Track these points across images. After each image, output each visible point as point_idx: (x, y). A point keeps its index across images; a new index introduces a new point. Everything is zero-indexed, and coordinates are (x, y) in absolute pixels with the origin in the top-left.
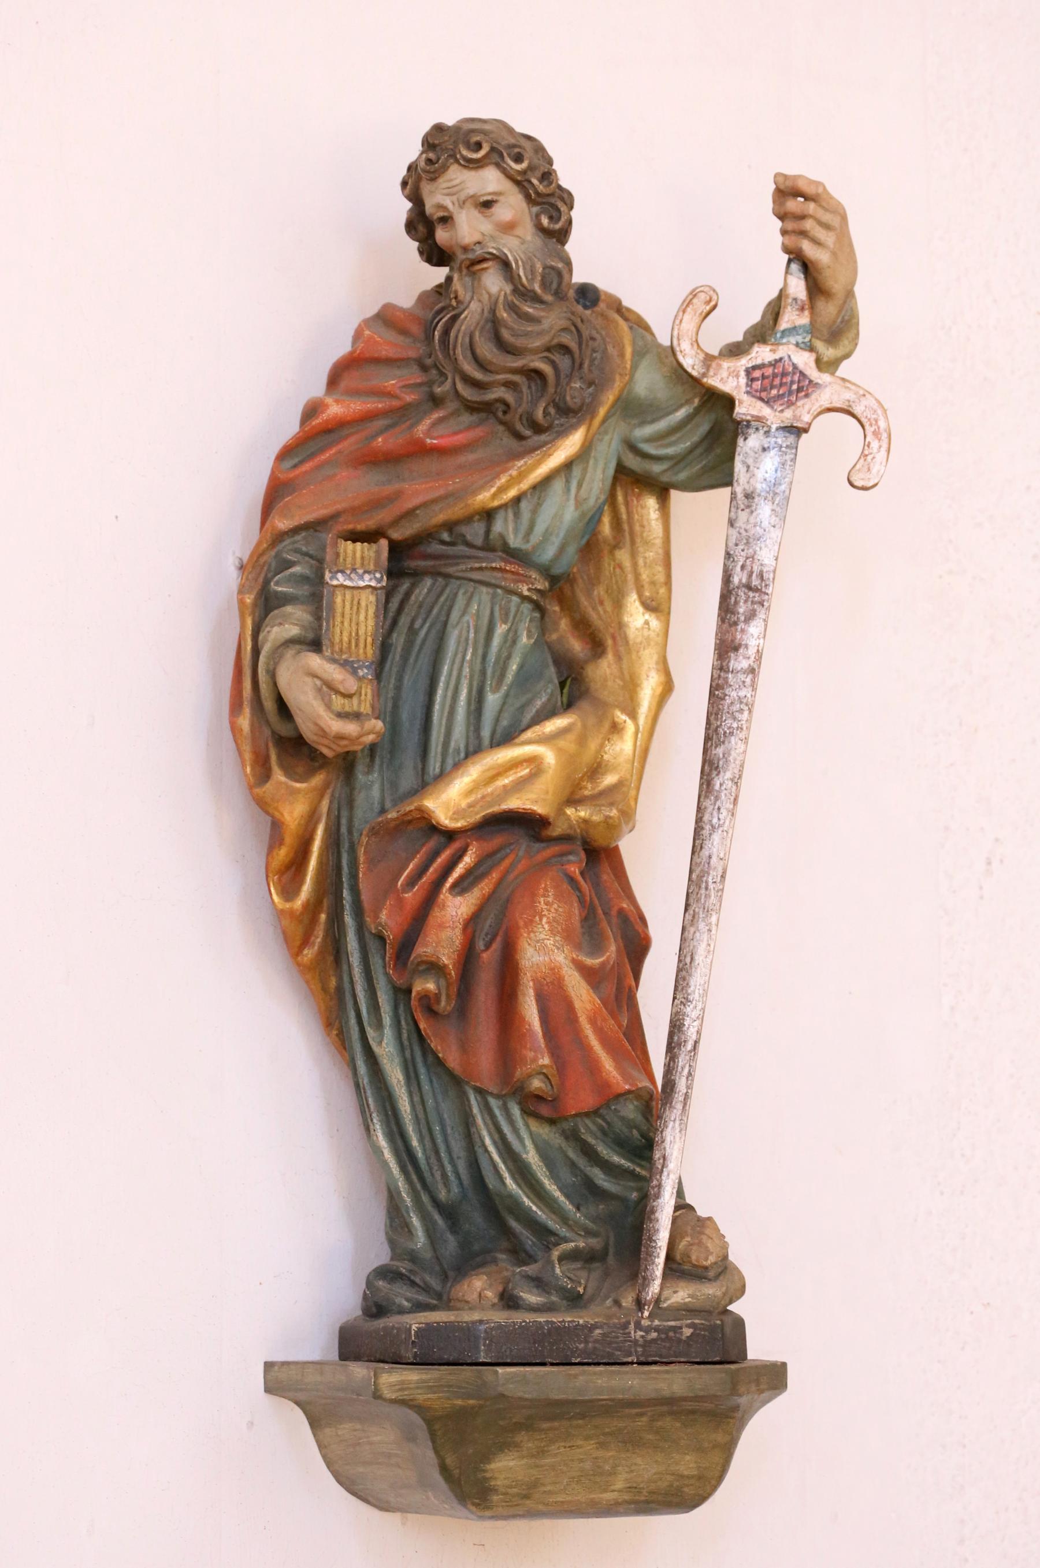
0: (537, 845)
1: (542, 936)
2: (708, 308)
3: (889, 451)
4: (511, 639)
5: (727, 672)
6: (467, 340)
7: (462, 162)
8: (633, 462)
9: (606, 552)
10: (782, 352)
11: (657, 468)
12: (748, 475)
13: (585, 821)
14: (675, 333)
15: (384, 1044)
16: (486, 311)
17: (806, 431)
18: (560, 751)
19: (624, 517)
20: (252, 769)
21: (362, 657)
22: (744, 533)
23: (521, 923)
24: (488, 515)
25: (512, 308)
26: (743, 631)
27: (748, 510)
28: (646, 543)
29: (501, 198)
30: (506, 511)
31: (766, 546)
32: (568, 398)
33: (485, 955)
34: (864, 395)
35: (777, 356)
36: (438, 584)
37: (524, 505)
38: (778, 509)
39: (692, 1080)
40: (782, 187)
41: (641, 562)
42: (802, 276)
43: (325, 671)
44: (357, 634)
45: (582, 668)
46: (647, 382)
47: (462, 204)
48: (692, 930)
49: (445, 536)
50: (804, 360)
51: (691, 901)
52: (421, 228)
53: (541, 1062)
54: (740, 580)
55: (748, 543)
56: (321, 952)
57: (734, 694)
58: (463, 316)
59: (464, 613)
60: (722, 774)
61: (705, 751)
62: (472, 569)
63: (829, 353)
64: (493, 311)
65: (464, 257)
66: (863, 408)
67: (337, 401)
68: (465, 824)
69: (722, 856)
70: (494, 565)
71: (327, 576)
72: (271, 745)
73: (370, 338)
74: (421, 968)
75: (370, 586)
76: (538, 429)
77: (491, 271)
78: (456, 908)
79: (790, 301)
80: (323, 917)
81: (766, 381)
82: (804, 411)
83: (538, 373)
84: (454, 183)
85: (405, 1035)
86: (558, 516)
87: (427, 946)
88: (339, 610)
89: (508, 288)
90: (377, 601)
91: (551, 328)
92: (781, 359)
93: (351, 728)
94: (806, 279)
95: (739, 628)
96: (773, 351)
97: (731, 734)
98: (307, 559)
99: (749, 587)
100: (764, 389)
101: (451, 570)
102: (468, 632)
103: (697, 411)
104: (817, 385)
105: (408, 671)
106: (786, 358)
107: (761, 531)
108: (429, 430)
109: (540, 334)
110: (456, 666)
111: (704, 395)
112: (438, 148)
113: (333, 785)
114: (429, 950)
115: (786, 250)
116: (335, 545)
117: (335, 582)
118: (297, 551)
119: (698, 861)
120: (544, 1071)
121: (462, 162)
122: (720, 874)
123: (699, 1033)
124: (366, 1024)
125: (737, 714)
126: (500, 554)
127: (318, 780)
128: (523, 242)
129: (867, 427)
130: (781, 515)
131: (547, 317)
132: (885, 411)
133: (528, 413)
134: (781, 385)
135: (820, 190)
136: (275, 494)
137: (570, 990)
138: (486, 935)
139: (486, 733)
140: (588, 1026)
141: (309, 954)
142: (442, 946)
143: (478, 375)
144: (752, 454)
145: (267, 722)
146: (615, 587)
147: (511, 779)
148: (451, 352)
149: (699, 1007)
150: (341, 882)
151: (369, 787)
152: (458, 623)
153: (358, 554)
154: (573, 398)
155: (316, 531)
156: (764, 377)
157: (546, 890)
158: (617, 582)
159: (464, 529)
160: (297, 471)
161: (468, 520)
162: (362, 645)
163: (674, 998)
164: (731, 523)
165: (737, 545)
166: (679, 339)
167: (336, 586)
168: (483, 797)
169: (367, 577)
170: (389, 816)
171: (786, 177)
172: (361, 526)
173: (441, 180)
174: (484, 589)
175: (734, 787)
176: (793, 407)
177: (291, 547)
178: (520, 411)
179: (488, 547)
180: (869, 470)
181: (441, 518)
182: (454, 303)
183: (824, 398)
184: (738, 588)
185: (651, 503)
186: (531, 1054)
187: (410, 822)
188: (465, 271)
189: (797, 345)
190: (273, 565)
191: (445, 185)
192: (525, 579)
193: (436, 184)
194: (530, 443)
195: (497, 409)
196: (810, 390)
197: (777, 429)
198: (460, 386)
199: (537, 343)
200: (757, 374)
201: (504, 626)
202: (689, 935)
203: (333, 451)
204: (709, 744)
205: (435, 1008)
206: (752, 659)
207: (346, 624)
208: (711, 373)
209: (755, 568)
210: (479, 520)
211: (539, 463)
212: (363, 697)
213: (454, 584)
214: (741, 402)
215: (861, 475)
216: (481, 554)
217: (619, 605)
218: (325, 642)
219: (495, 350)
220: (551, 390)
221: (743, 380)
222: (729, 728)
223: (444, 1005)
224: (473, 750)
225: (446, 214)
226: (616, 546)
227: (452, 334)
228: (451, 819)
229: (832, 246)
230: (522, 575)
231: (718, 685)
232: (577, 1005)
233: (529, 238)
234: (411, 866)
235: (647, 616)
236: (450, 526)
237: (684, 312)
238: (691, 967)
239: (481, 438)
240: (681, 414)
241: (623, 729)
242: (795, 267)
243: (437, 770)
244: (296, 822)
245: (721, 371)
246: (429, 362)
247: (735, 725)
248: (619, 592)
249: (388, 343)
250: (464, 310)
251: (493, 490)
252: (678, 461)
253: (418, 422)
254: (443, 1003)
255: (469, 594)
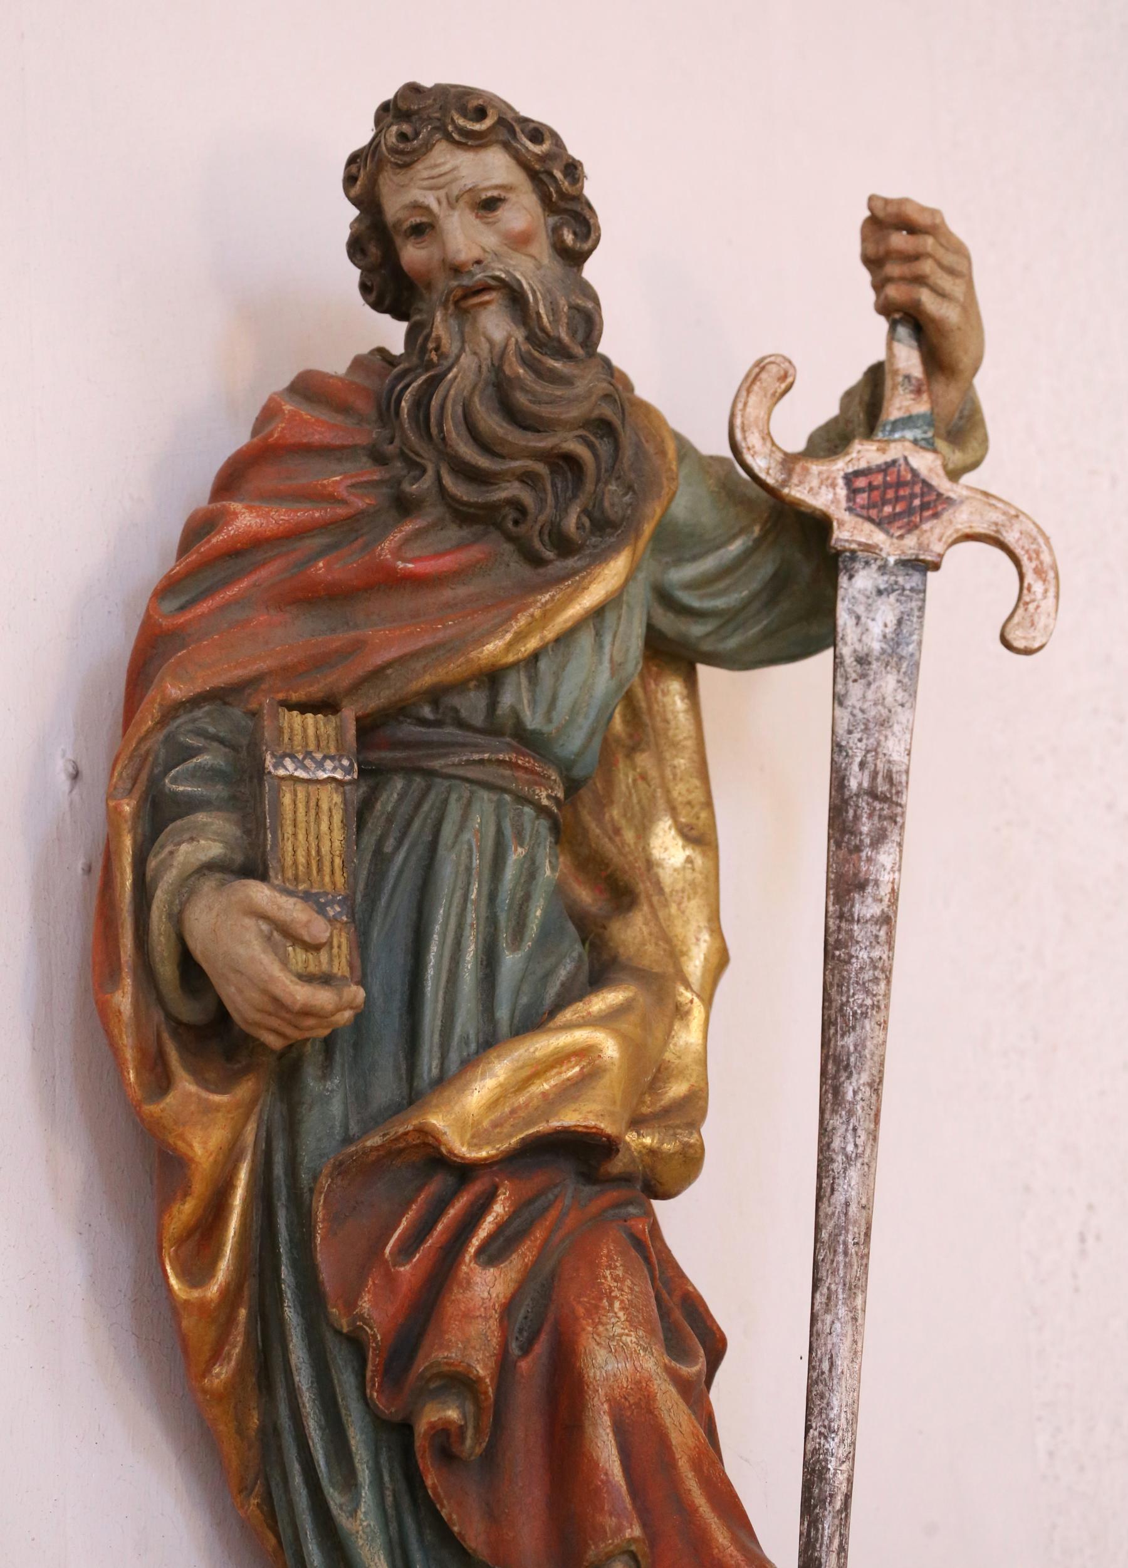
0: (588, 1190)
1: (618, 1330)
2: (783, 386)
3: (1057, 597)
4: (531, 872)
5: (851, 921)
6: (460, 410)
7: (456, 136)
8: (667, 622)
9: (620, 756)
10: (894, 452)
11: (697, 630)
12: (859, 630)
13: (652, 1152)
14: (738, 422)
15: (361, 1515)
16: (484, 369)
17: (936, 567)
18: (624, 1040)
19: (643, 705)
20: (138, 1074)
21: (329, 887)
22: (860, 715)
23: (581, 1311)
24: (492, 678)
25: (527, 361)
26: (869, 860)
27: (863, 681)
28: (674, 745)
29: (511, 196)
30: (518, 672)
31: (893, 734)
32: (606, 504)
33: (523, 1365)
34: (1017, 516)
35: (888, 457)
36: (415, 786)
37: (543, 665)
38: (906, 680)
39: (846, 1557)
40: (881, 214)
41: (668, 773)
42: (915, 344)
43: (280, 908)
44: (318, 852)
45: (604, 927)
46: (686, 502)
47: (452, 203)
48: (828, 1318)
49: (427, 712)
50: (925, 463)
51: (823, 1273)
52: (373, 250)
53: (628, 1534)
54: (860, 784)
55: (866, 729)
56: (240, 1371)
57: (863, 955)
58: (450, 376)
59: (462, 827)
60: (855, 1076)
61: (825, 1043)
62: (469, 763)
63: (958, 458)
64: (497, 368)
65: (455, 283)
66: (1017, 535)
67: (250, 508)
68: (493, 1152)
69: (864, 1202)
70: (501, 756)
71: (269, 762)
72: (166, 1036)
73: (293, 415)
74: (432, 1386)
75: (334, 779)
76: (565, 546)
77: (493, 307)
78: (486, 1286)
79: (900, 379)
80: (243, 1312)
81: (876, 493)
82: (933, 536)
83: (571, 461)
84: (443, 169)
85: (389, 1500)
86: (587, 687)
87: (448, 1348)
88: (288, 815)
89: (519, 334)
90: (345, 802)
91: (590, 393)
92: (894, 462)
93: (323, 997)
94: (921, 347)
95: (864, 854)
96: (882, 450)
97: (865, 1015)
98: (215, 744)
99: (873, 794)
100: (871, 505)
101: (437, 764)
102: (470, 857)
103: (758, 543)
104: (949, 501)
105: (378, 918)
106: (902, 461)
107: (884, 712)
108: (399, 548)
109: (571, 401)
110: (454, 911)
111: (766, 522)
112: (415, 118)
113: (261, 1101)
114: (454, 1354)
115: (885, 308)
116: (276, 717)
117: (281, 772)
118: (201, 733)
119: (829, 1210)
120: (633, 1548)
121: (456, 136)
122: (863, 1230)
123: (850, 1481)
124: (325, 1482)
125: (870, 985)
126: (508, 739)
127: (244, 1090)
128: (539, 267)
129: (1025, 560)
130: (909, 686)
131: (582, 377)
132: (1047, 540)
133: (552, 523)
134: (897, 499)
135: (938, 221)
136: (151, 651)
137: (665, 1415)
138: (521, 1331)
139: (503, 1013)
140: (690, 1475)
141: (222, 1373)
142: (474, 1348)
143: (483, 462)
144: (862, 598)
145: (161, 1001)
146: (637, 808)
147: (553, 1083)
148: (434, 431)
149: (848, 1441)
150: (277, 1256)
151: (325, 1100)
152: (454, 843)
153: (311, 731)
154: (613, 505)
155: (225, 703)
156: (871, 487)
157: (609, 1257)
158: (639, 801)
159: (455, 701)
160: (189, 615)
161: (459, 686)
162: (327, 870)
163: (808, 1428)
164: (838, 699)
165: (850, 732)
166: (744, 431)
167: (283, 778)
168: (513, 1112)
169: (329, 764)
170: (369, 1143)
171: (887, 202)
172: (315, 689)
173: (419, 166)
174: (485, 795)
175: (874, 1097)
176: (917, 532)
177: (190, 727)
178: (542, 518)
179: (493, 729)
180: (1033, 624)
181: (427, 680)
182: (434, 357)
183: (963, 518)
184: (858, 795)
185: (675, 687)
186: (611, 1522)
187: (401, 1151)
188: (451, 308)
189: (915, 442)
190: (162, 753)
191: (425, 174)
192: (542, 780)
193: (411, 172)
194: (551, 570)
195: (504, 517)
196: (940, 508)
197: (897, 563)
198: (448, 481)
199: (574, 413)
200: (861, 482)
201: (520, 850)
202: (823, 1327)
203: (244, 584)
204: (832, 1031)
205: (455, 1449)
206: (886, 899)
207: (301, 836)
208: (795, 480)
209: (880, 766)
210: (477, 687)
211: (569, 600)
212: (335, 950)
213: (441, 785)
214: (841, 524)
215: (1019, 633)
216: (480, 739)
217: (644, 830)
218: (272, 863)
219: (505, 424)
220: (589, 486)
221: (842, 492)
222: (861, 1006)
223: (471, 1446)
224: (490, 1042)
225: (424, 219)
226: (632, 750)
227: (435, 403)
228: (471, 1145)
229: (962, 299)
230: (538, 774)
231: (837, 941)
232: (675, 1438)
233: (546, 261)
234: (404, 1223)
235: (689, 852)
236: (435, 695)
237: (749, 391)
238: (831, 1378)
239: (478, 562)
240: (736, 547)
241: (688, 1013)
242: (902, 331)
243: (435, 1071)
244: (211, 1159)
245: (808, 478)
246: (390, 449)
247: (869, 1002)
248: (644, 816)
249: (319, 425)
250: (450, 369)
251: (508, 637)
252: (730, 619)
253: (382, 537)
254: (468, 1442)
255: (465, 800)
